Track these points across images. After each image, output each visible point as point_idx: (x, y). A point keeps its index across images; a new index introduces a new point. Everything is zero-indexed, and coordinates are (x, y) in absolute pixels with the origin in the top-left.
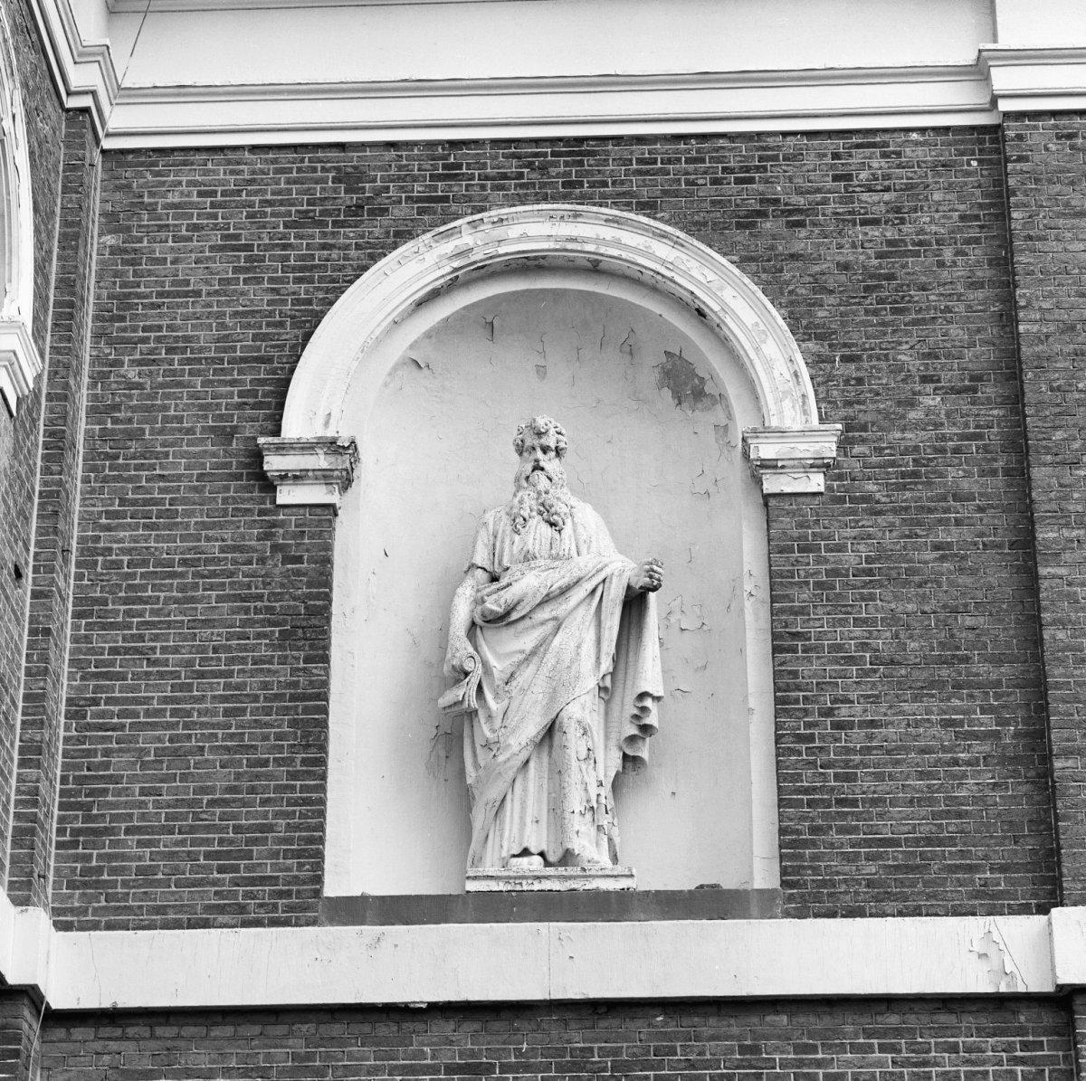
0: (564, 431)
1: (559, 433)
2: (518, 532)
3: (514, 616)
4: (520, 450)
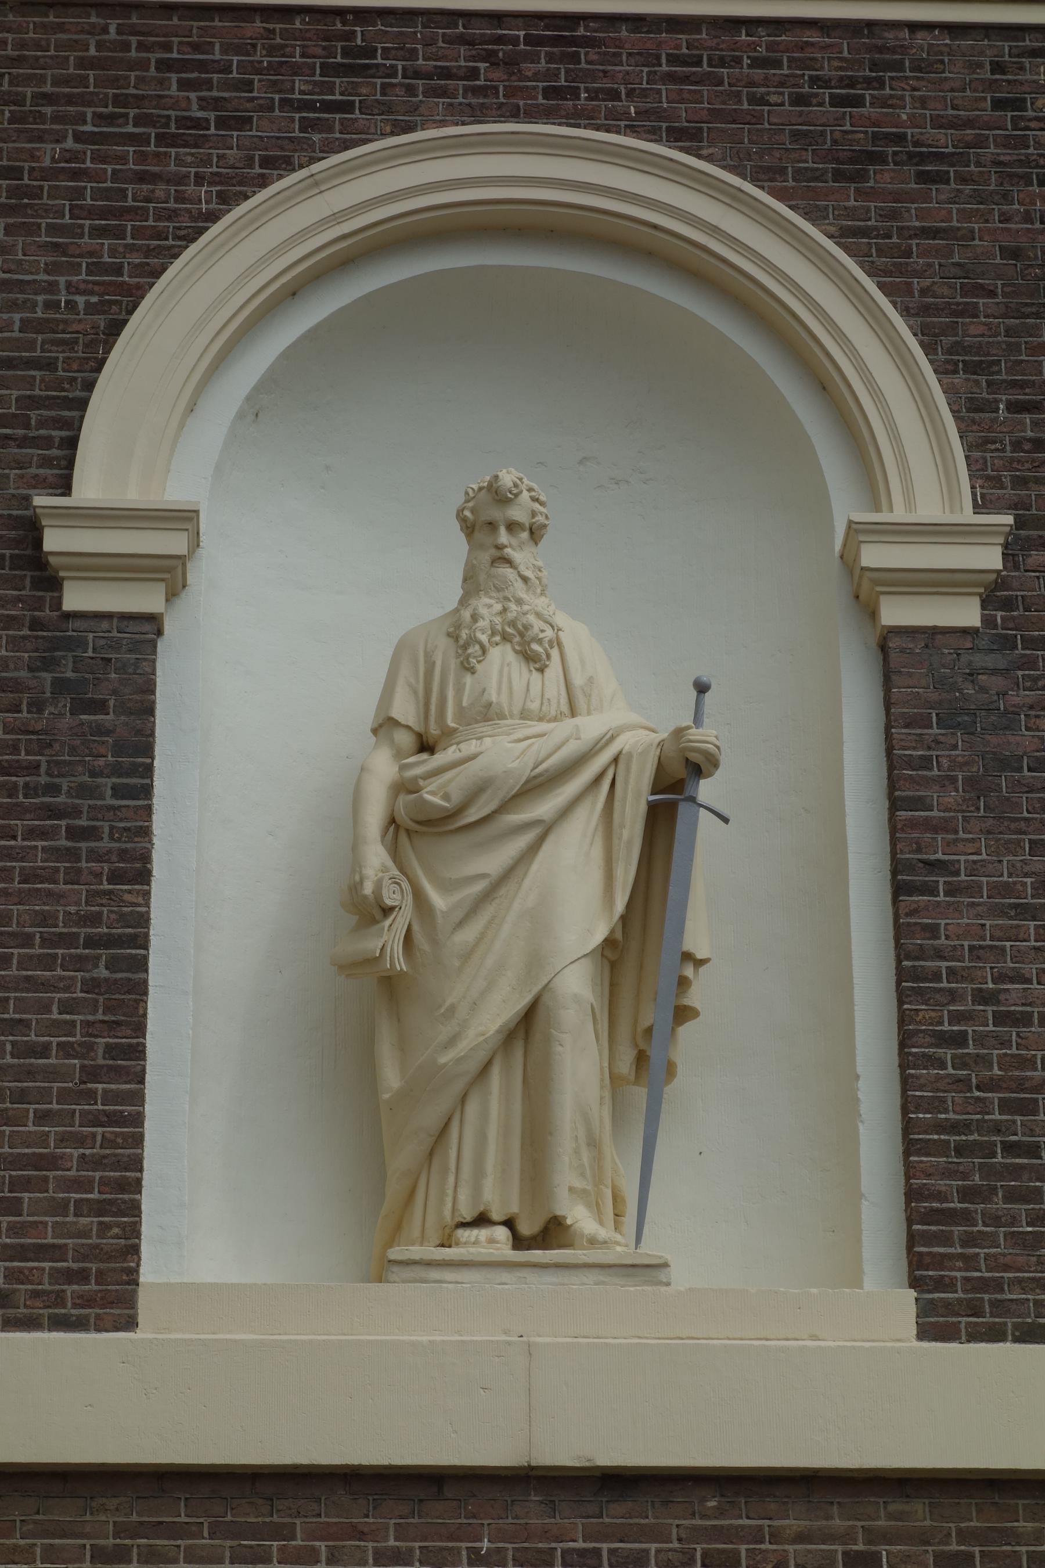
0: (543, 498)
1: (537, 500)
2: (472, 671)
3: (473, 815)
4: (469, 529)
